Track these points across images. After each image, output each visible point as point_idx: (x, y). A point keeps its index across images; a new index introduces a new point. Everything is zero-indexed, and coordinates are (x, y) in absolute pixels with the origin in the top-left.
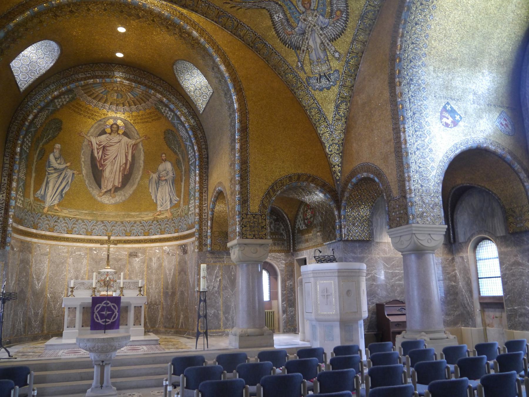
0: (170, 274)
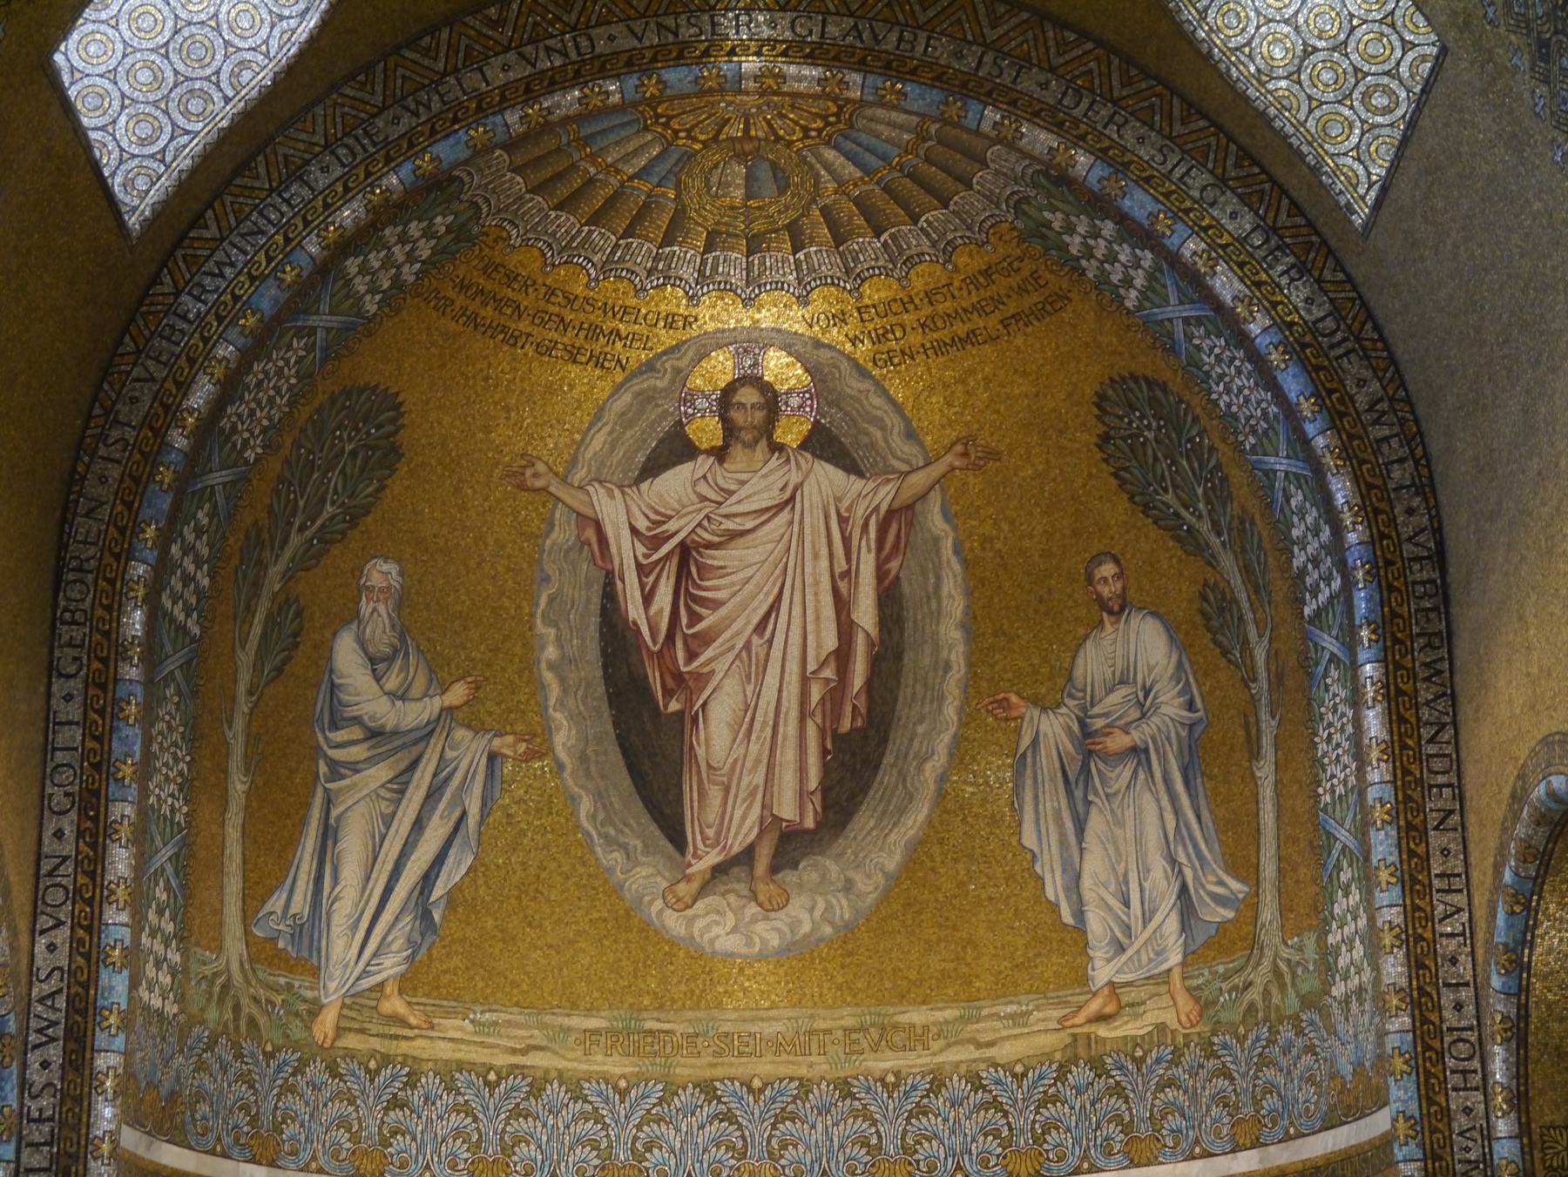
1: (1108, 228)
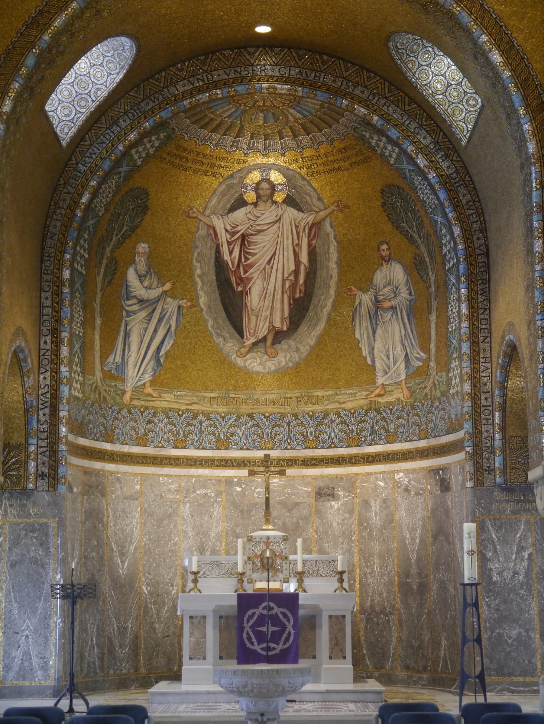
0: (413, 539)
1: (384, 139)
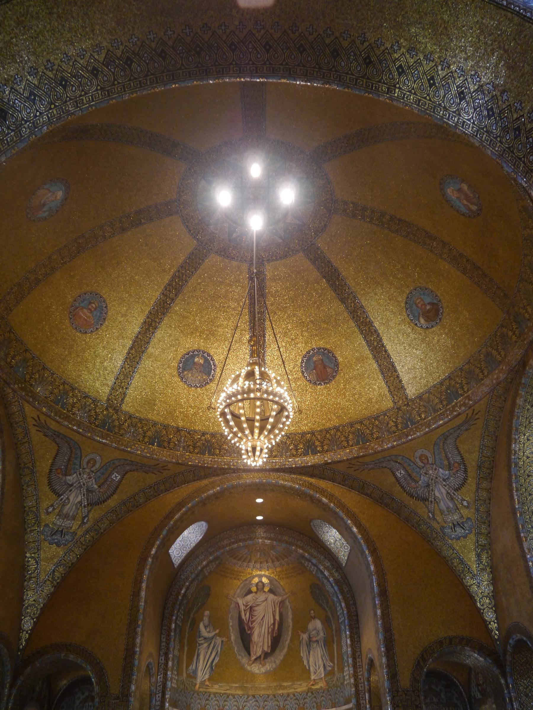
1: (310, 563)
